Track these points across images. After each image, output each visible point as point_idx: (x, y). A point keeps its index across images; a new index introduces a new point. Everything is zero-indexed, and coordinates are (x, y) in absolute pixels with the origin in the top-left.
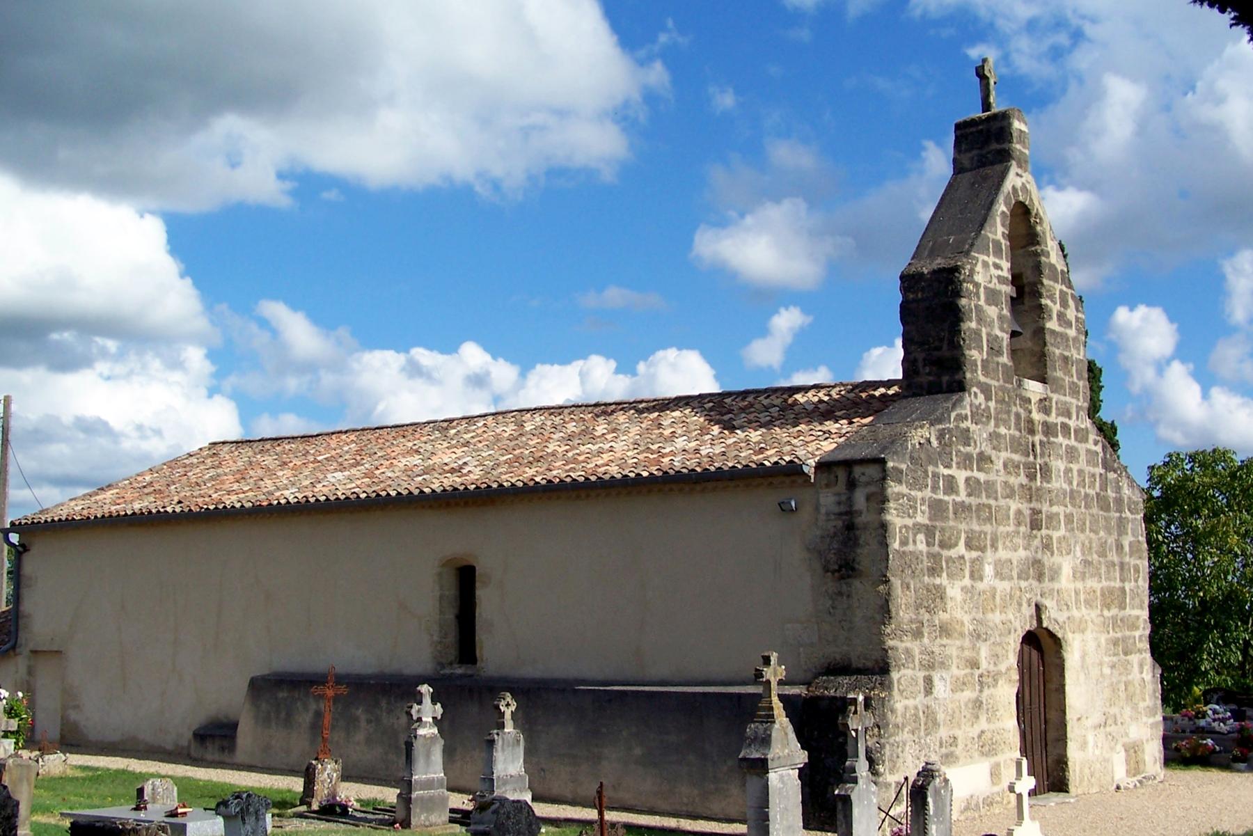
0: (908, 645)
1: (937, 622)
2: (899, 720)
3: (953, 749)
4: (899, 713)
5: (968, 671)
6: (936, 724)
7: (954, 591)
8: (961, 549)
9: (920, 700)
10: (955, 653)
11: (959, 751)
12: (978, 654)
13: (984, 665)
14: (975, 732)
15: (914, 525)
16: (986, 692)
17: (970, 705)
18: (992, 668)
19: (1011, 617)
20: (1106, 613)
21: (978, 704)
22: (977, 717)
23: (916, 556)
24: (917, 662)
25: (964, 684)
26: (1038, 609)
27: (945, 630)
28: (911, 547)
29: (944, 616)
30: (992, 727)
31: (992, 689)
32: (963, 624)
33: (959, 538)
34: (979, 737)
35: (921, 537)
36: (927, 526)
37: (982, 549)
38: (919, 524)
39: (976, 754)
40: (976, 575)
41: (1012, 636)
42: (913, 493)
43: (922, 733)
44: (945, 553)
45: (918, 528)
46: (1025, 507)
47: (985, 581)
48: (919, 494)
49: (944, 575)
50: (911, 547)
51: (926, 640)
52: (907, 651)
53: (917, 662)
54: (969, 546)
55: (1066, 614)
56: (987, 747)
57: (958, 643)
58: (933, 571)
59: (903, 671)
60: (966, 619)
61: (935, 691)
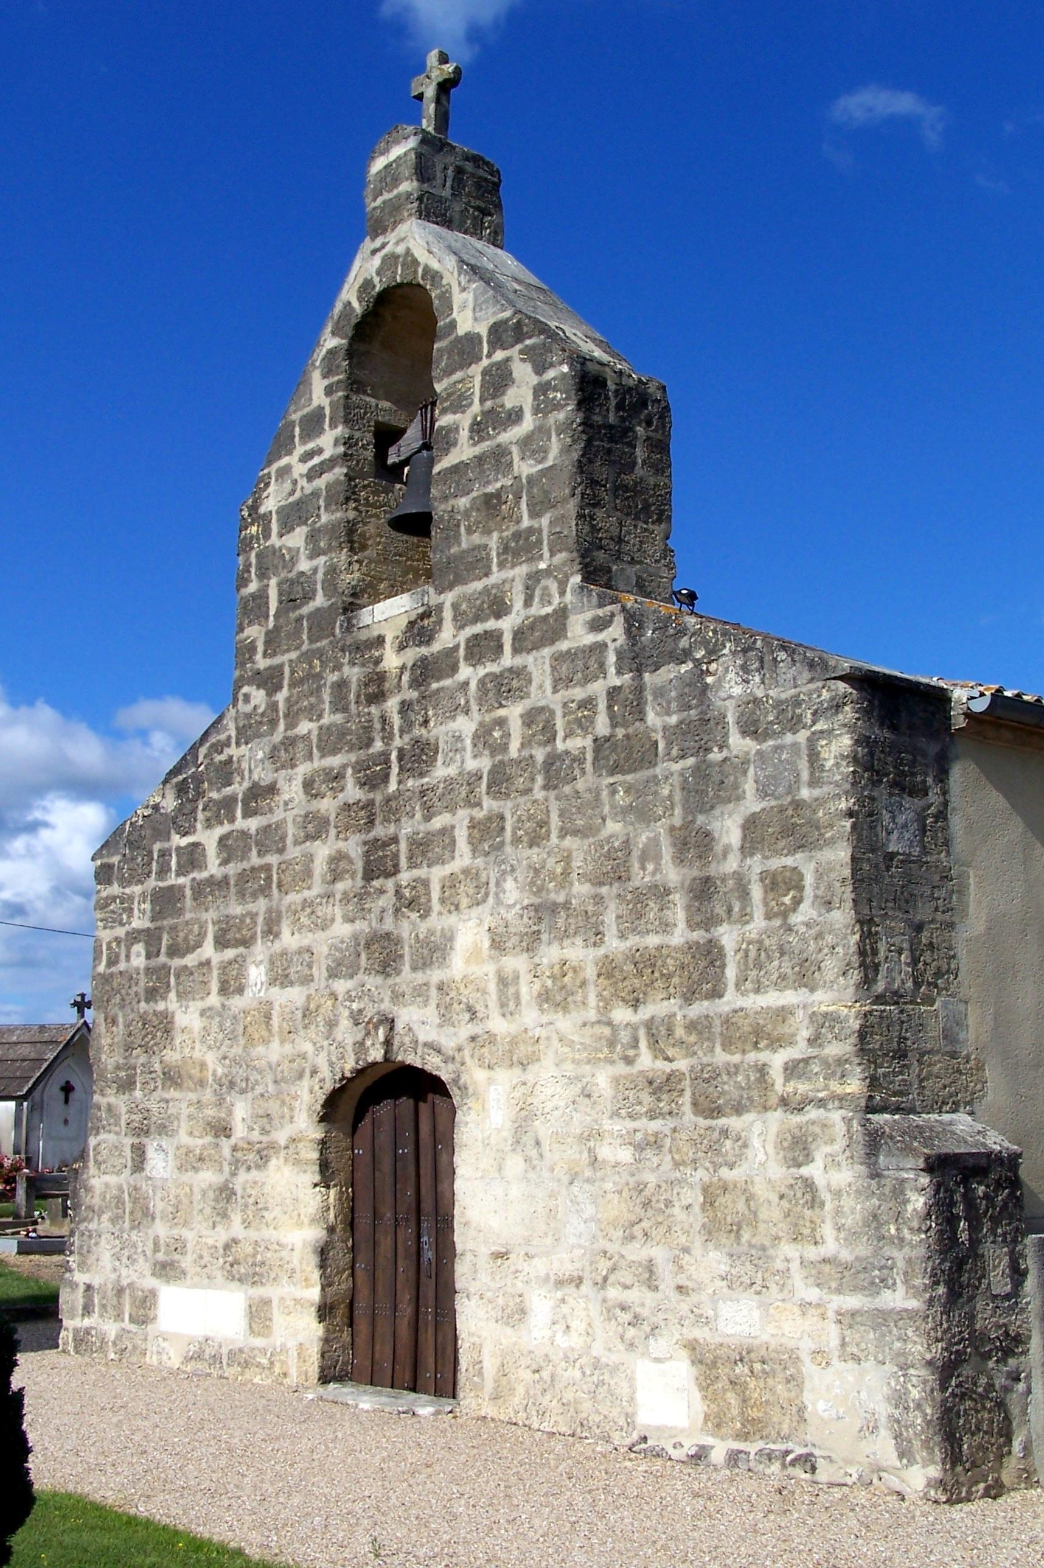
0: (112, 1100)
1: (157, 1067)
2: (96, 1201)
3: (176, 1257)
4: (97, 1192)
5: (209, 1139)
6: (148, 1215)
7: (188, 1018)
8: (208, 950)
9: (125, 1178)
10: (185, 1111)
11: (187, 1262)
12: (230, 1113)
13: (240, 1132)
14: (221, 1236)
15: (127, 933)
16: (243, 1176)
17: (211, 1195)
18: (255, 1136)
19: (308, 1047)
20: (622, 1014)
21: (226, 1193)
22: (224, 1215)
23: (129, 977)
24: (123, 1123)
25: (201, 1159)
26: (67, 1101)
27: (172, 1078)
28: (122, 966)
29: (172, 1056)
30: (253, 1234)
31: (254, 1172)
32: (203, 1065)
33: (202, 935)
34: (227, 1247)
35: (139, 948)
36: (148, 930)
37: (247, 943)
38: (135, 931)
39: (219, 1275)
40: (231, 986)
41: (306, 1082)
42: (127, 891)
43: (127, 1225)
44: (176, 963)
45: (134, 937)
46: (353, 846)
47: (249, 993)
48: (137, 889)
49: (172, 995)
50: (122, 966)
51: (138, 1094)
52: (110, 1108)
53: (123, 1123)
54: (221, 943)
55: (466, 1030)
56: (243, 1267)
57: (193, 1096)
58: (152, 994)
59: (103, 1136)
60: (211, 1058)
61: (148, 1167)
